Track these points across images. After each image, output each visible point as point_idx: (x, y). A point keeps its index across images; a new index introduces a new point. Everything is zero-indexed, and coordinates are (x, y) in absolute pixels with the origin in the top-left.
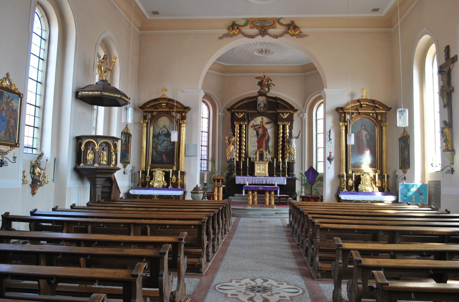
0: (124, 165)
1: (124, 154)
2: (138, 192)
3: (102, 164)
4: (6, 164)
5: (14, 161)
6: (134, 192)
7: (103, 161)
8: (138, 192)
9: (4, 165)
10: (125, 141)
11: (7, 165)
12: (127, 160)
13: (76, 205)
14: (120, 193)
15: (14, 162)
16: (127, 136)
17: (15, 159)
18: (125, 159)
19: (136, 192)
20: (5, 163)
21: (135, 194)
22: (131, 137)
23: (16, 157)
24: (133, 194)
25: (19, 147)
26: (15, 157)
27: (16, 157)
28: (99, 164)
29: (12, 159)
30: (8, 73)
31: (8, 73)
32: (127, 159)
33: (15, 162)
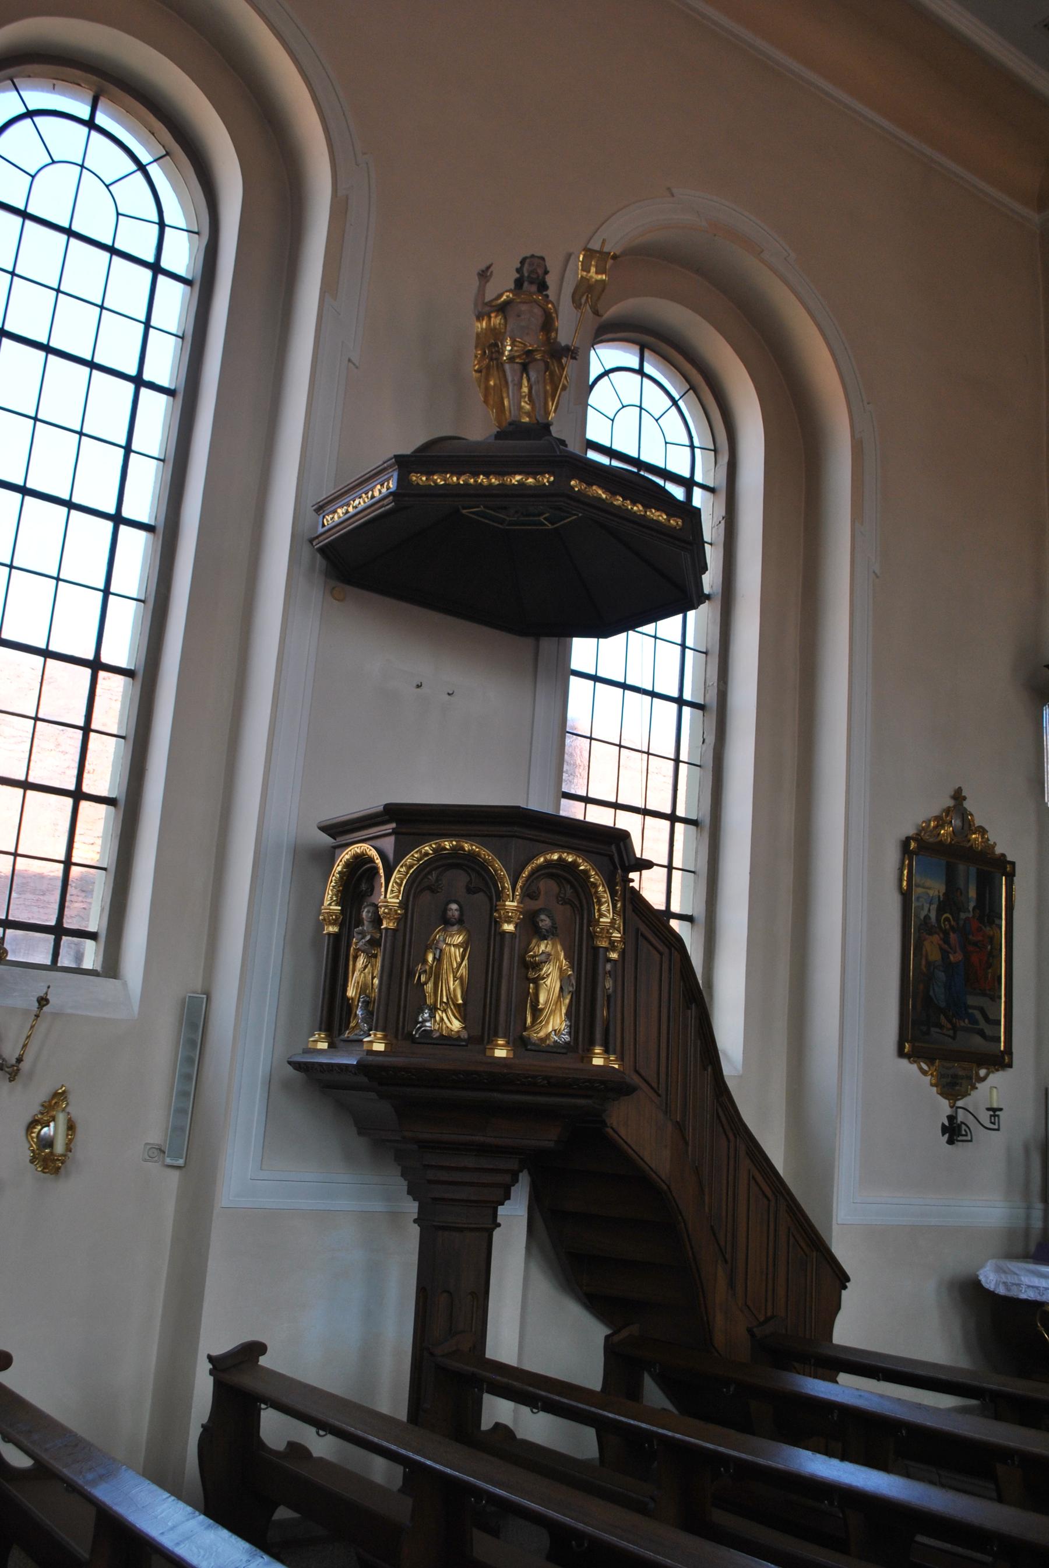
0: (941, 1076)
1: (939, 993)
2: (1036, 1281)
3: (428, 1033)
4: (966, 1135)
5: (994, 1123)
6: (1010, 1279)
7: (433, 1009)
8: (1036, 1281)
9: (960, 1138)
10: (949, 903)
11: (969, 1138)
12: (978, 1040)
13: (263, 1361)
14: (842, 1279)
15: (992, 1126)
16: (966, 875)
17: (995, 1116)
18: (955, 1028)
19: (1026, 1280)
20: (964, 1133)
21: (1014, 1293)
22: (1011, 876)
23: (1001, 1110)
24: (1001, 1291)
25: (1010, 1065)
26: (994, 1110)
27: (1001, 1110)
28: (521, 1043)
29: (985, 1117)
30: (959, 790)
31: (959, 790)
32: (982, 1033)
33: (996, 1127)
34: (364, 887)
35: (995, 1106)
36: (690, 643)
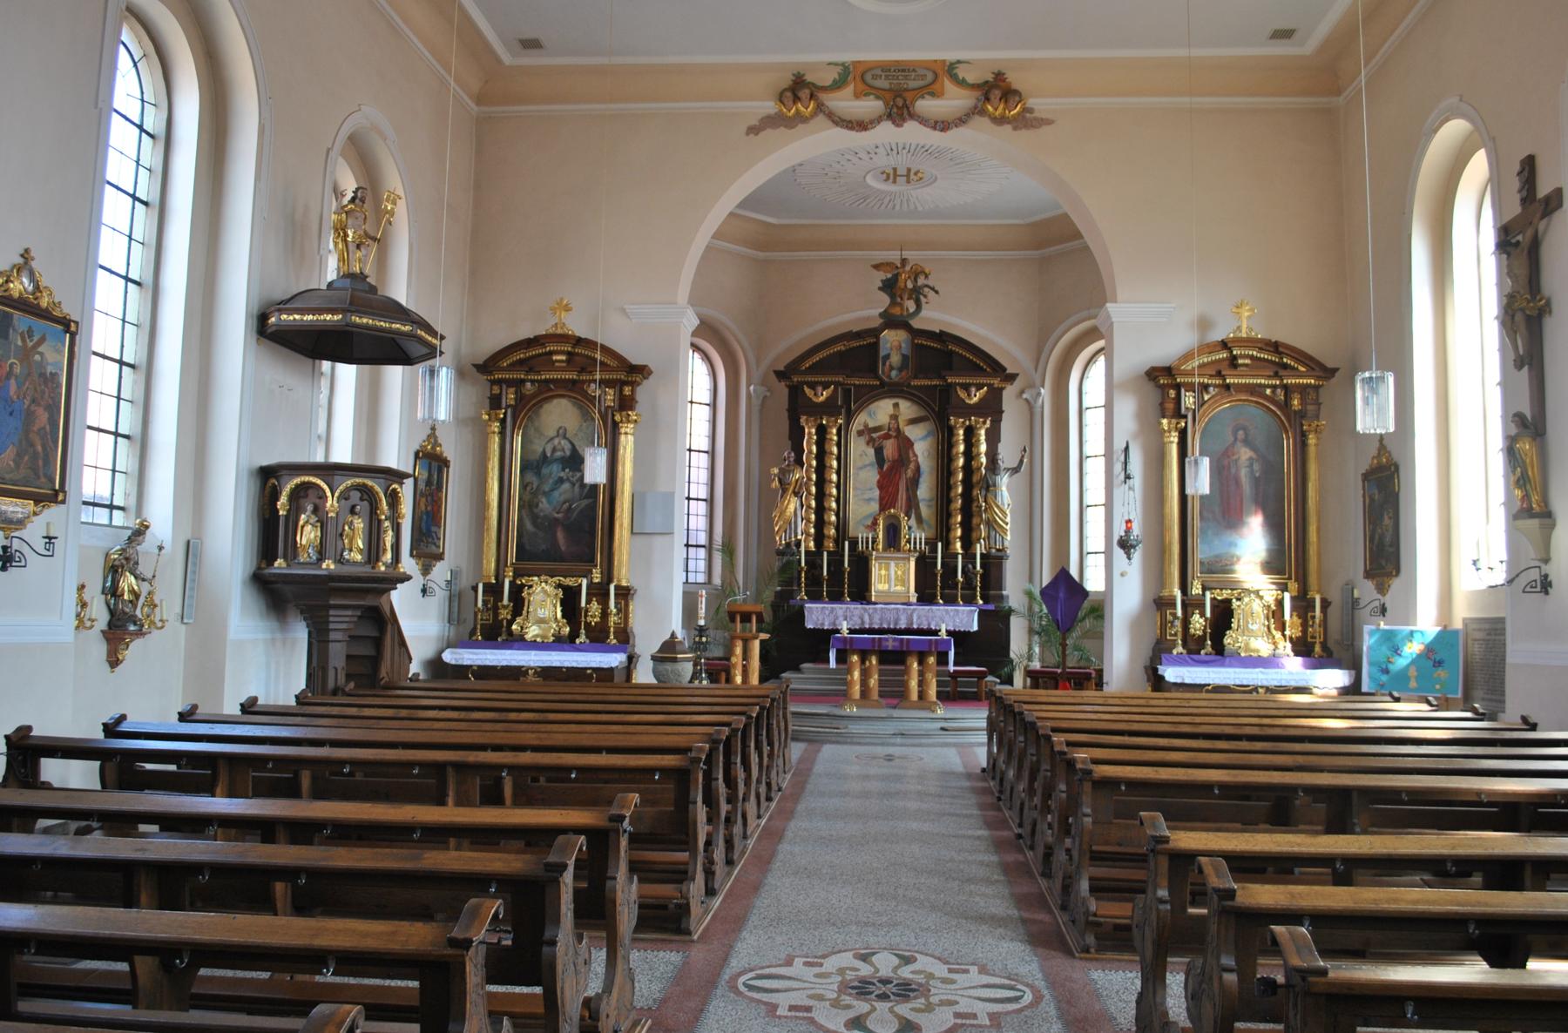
0: (423, 565)
1: (423, 525)
2: (471, 656)
3: (348, 561)
4: (20, 561)
5: (48, 550)
6: (458, 656)
8: (471, 656)
9: (14, 564)
11: (23, 564)
12: (434, 547)
13: (259, 702)
14: (410, 659)
15: (47, 553)
16: (435, 465)
17: (50, 543)
18: (428, 542)
19: (466, 656)
20: (17, 559)
21: (460, 663)
22: (448, 467)
23: (56, 538)
24: (453, 662)
25: (63, 502)
26: (50, 538)
27: (56, 538)
28: (340, 560)
29: (40, 545)
30: (27, 251)
31: (27, 251)
32: (435, 544)
33: (50, 553)
34: (302, 494)
35: (52, 535)
36: (137, 235)
